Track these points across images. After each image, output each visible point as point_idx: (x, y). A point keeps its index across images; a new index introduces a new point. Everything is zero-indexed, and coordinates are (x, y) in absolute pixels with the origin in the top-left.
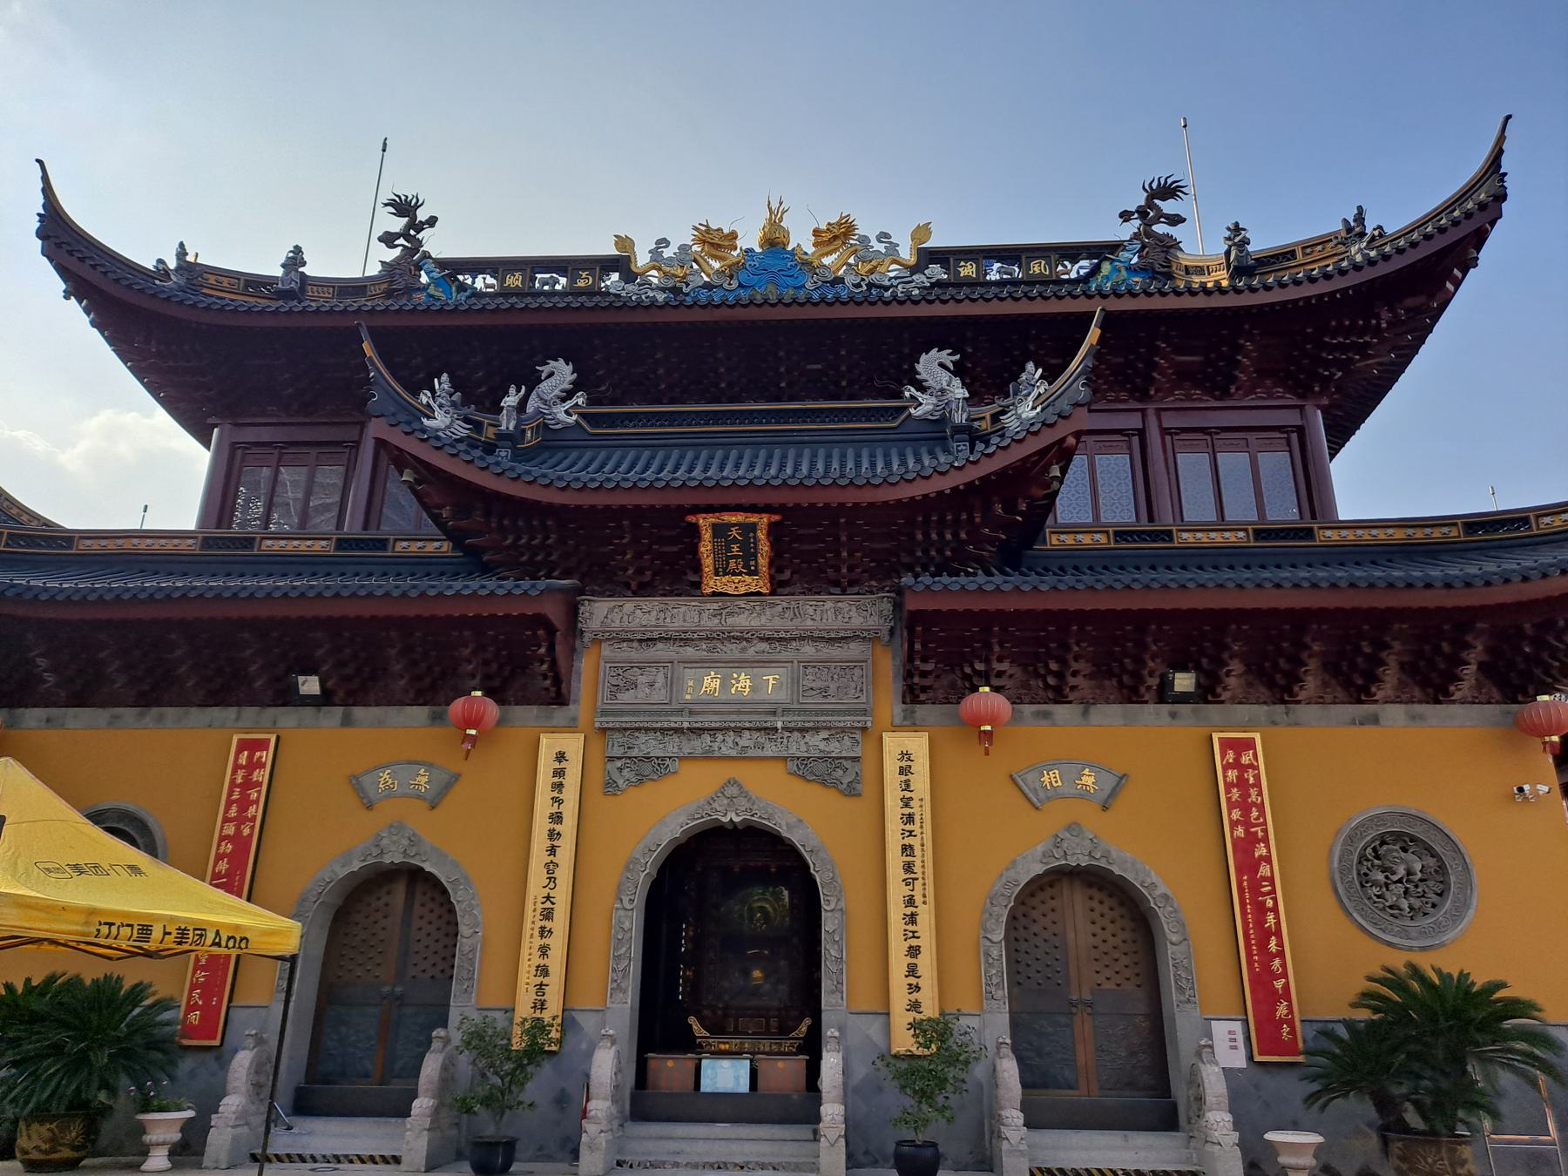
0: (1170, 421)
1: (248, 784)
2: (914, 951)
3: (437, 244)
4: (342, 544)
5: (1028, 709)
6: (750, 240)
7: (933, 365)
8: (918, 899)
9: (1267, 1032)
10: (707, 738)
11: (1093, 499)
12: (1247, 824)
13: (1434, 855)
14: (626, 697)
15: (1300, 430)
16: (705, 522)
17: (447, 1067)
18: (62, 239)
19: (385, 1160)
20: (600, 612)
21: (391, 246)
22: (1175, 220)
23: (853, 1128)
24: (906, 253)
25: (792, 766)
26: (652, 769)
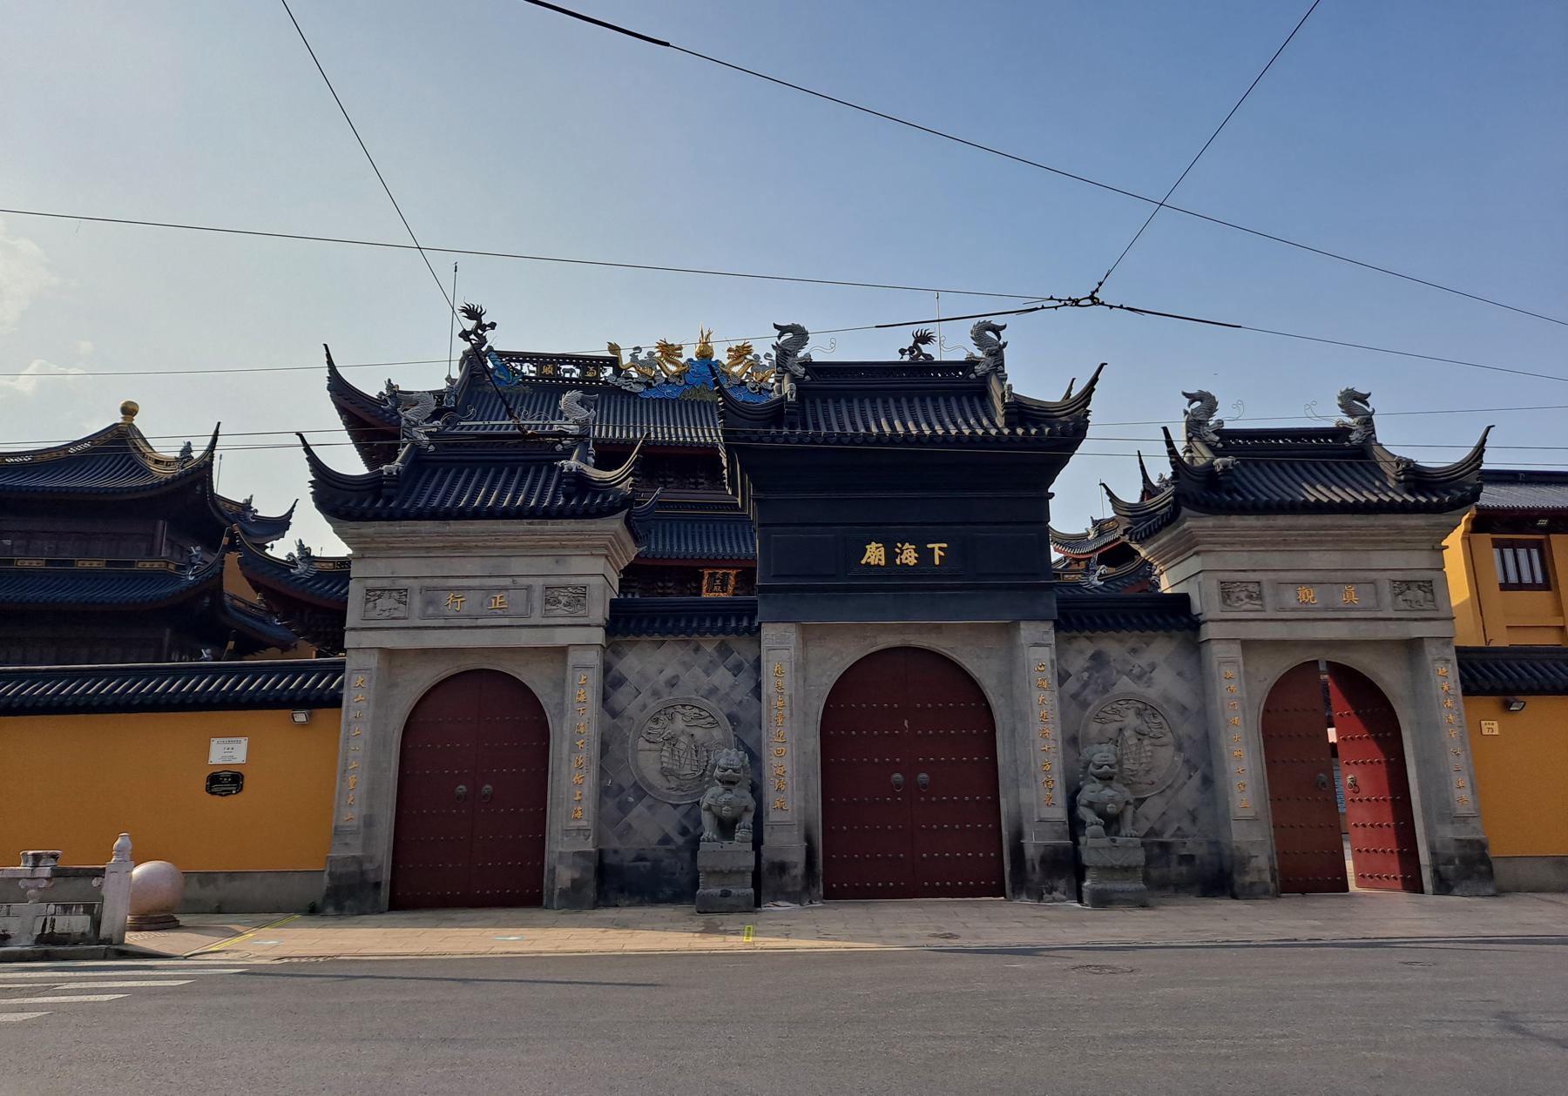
18: (340, 389)
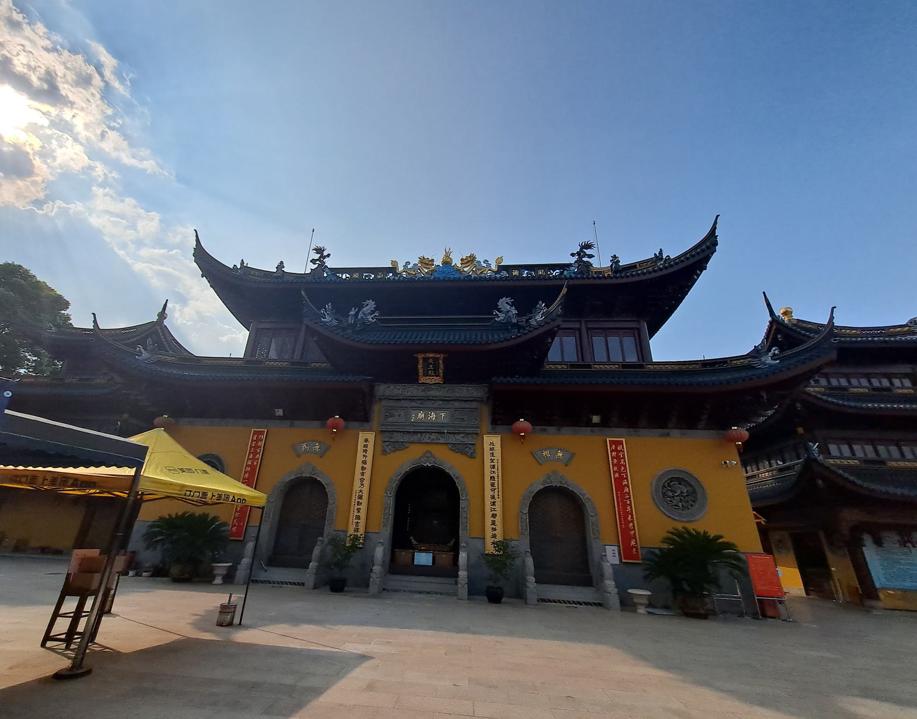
0: (590, 325)
1: (256, 447)
2: (494, 516)
3: (330, 263)
4: (293, 364)
5: (538, 427)
6: (438, 262)
7: (504, 303)
8: (496, 496)
9: (627, 551)
10: (419, 435)
11: (562, 352)
12: (620, 473)
13: (691, 486)
14: (390, 419)
15: (638, 329)
16: (420, 356)
17: (322, 551)
18: (202, 257)
19: (299, 584)
20: (382, 389)
21: (315, 264)
22: (591, 256)
23: (471, 581)
24: (494, 267)
25: (450, 446)
26: (399, 446)
